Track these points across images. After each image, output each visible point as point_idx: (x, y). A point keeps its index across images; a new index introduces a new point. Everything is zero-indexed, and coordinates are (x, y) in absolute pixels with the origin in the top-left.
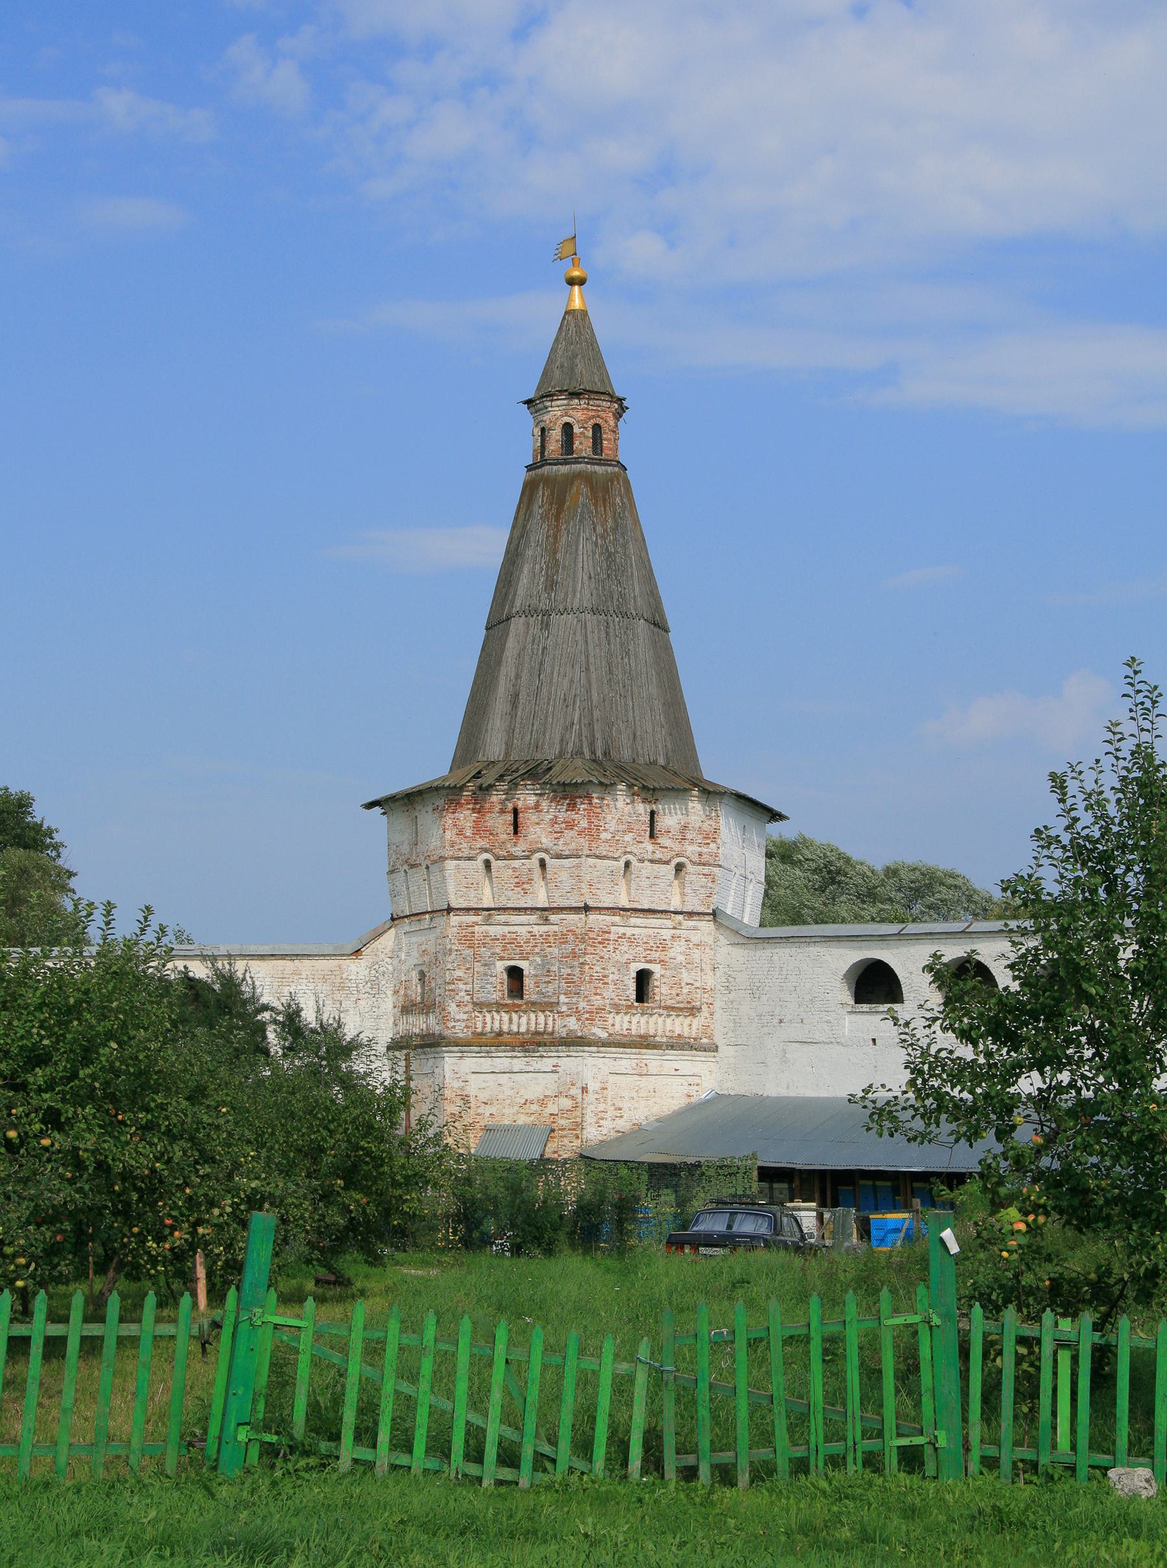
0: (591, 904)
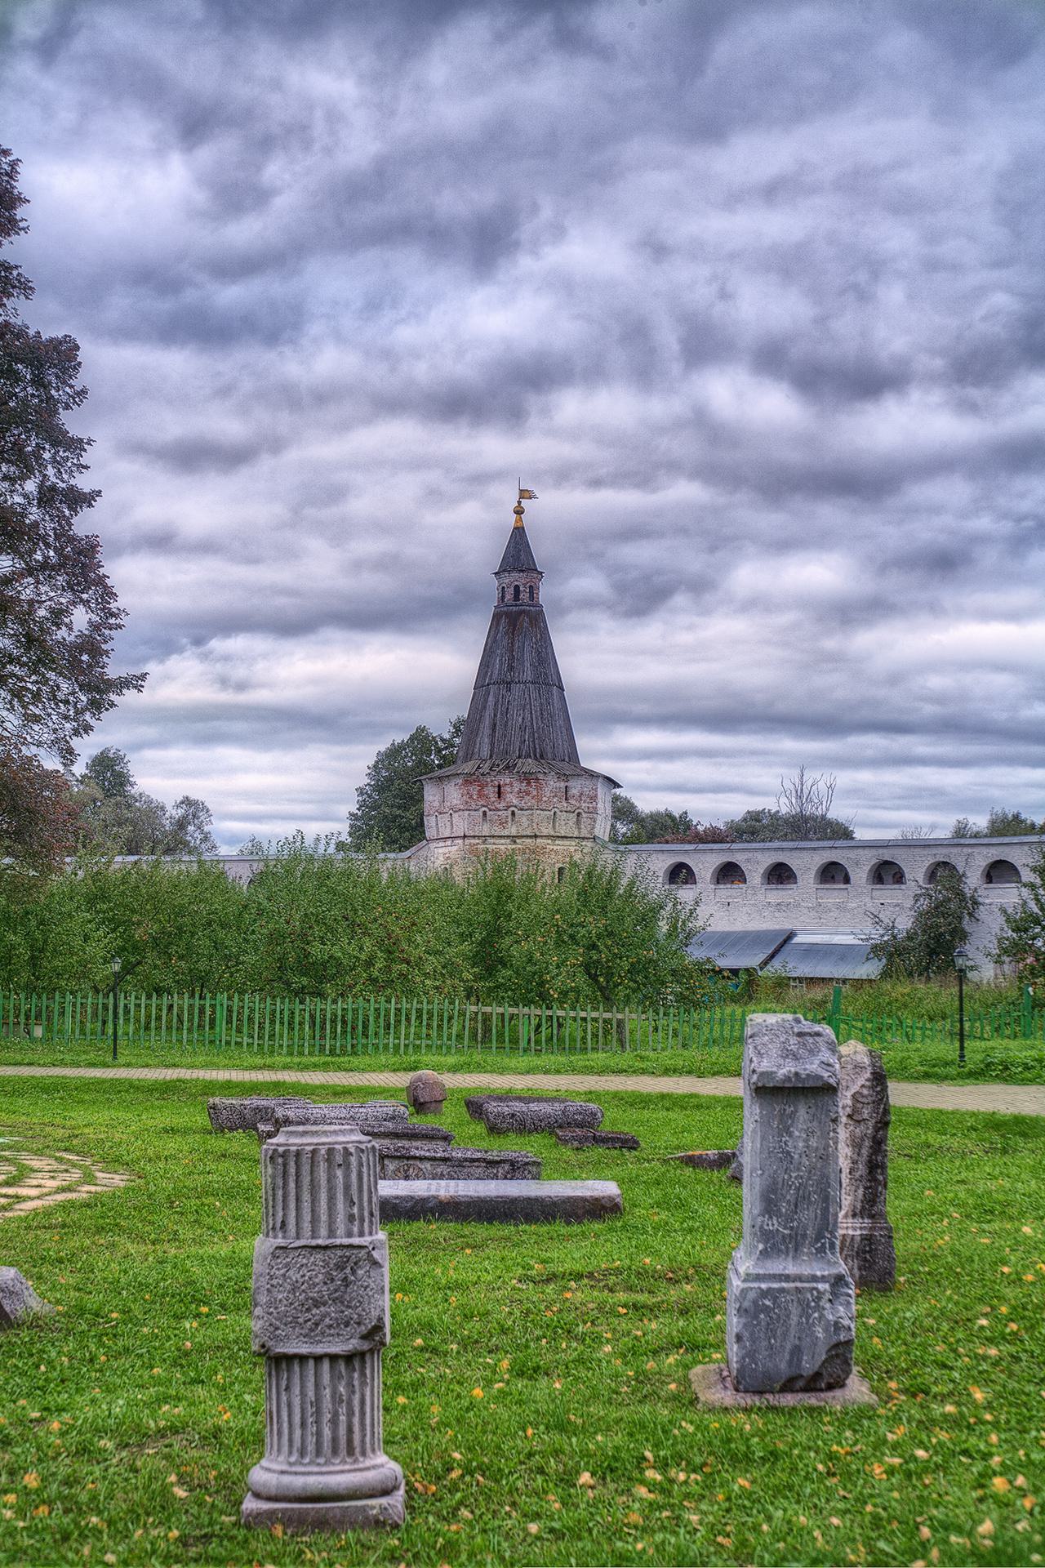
0: (538, 834)
